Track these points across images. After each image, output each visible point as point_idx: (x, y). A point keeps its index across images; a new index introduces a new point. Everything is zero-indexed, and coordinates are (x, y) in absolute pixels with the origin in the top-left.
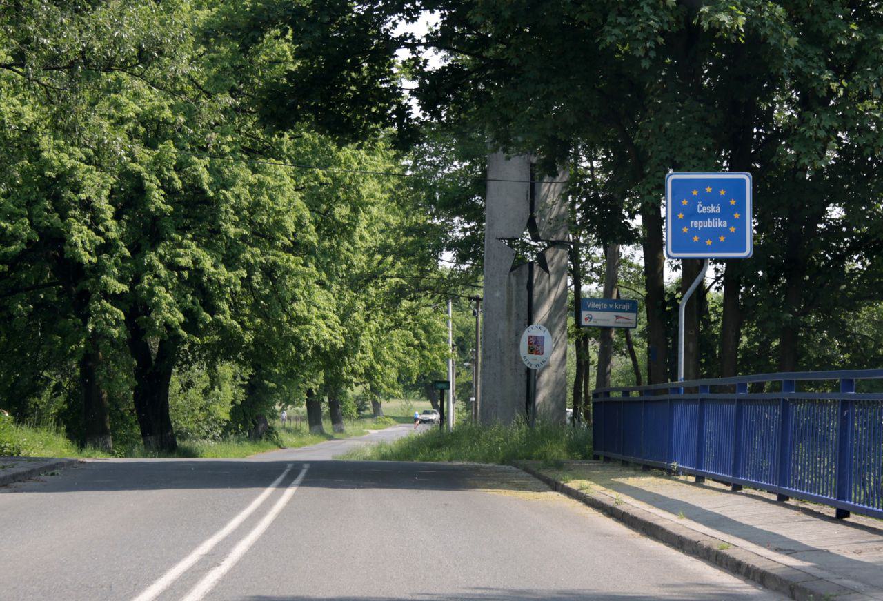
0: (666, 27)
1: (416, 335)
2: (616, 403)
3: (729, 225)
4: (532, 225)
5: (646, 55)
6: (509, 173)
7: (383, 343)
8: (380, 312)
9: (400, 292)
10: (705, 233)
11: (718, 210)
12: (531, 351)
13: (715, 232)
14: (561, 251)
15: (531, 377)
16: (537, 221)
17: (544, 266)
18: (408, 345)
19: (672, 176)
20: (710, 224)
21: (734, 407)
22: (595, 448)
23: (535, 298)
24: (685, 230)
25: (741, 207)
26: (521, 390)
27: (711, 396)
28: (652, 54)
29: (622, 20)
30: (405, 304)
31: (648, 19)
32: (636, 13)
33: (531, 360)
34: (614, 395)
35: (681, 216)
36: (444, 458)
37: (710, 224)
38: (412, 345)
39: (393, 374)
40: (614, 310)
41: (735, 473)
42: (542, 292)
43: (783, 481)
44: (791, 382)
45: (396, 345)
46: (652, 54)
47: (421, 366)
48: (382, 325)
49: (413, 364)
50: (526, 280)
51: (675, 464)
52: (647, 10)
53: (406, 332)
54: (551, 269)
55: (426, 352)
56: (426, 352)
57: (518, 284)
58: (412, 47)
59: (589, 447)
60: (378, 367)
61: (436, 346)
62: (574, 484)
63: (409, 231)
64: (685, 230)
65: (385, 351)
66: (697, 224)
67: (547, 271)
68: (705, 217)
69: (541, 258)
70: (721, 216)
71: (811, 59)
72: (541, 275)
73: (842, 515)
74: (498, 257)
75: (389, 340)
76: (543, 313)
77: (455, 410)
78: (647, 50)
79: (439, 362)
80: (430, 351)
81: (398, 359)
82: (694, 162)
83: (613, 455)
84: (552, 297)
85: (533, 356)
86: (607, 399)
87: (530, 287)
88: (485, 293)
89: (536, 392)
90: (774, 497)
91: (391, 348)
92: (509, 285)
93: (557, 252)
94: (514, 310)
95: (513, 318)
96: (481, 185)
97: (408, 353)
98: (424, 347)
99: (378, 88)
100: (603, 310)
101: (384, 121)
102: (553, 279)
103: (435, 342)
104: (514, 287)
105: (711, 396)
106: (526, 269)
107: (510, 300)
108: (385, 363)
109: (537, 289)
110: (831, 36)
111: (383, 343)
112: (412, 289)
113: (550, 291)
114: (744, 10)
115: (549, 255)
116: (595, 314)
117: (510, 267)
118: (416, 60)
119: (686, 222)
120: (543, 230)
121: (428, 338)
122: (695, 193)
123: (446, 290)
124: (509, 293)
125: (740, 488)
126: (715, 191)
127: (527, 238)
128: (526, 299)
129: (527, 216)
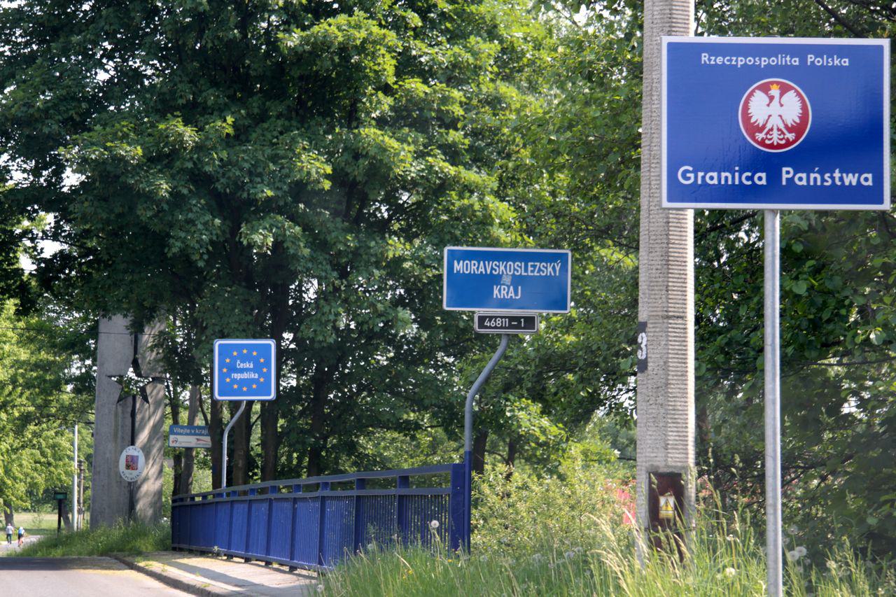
0: (215, 238)
1: (43, 454)
2: (198, 505)
3: (259, 377)
4: (136, 365)
5: (201, 258)
6: (116, 328)
7: (13, 461)
8: (11, 434)
9: (26, 419)
10: (242, 382)
11: (252, 366)
12: (128, 467)
13: (248, 382)
14: (159, 386)
15: (132, 490)
16: (140, 361)
17: (145, 399)
18: (36, 462)
19: (218, 343)
20: (245, 376)
21: (246, 506)
22: (173, 542)
23: (137, 424)
24: (228, 380)
25: (268, 364)
26: (124, 500)
27: (260, 497)
28: (206, 257)
29: (182, 235)
30: (32, 427)
31: (202, 234)
32: (193, 229)
33: (128, 475)
34: (198, 499)
35: (225, 370)
36: (58, 553)
37: (245, 376)
38: (40, 463)
39: (22, 488)
40: (195, 434)
41: (247, 550)
42: (143, 419)
43: (268, 553)
44: (327, 483)
45: (24, 462)
46: (206, 257)
47: (46, 480)
48: (11, 446)
49: (40, 479)
50: (129, 410)
51: (216, 548)
52: (200, 226)
53: (34, 451)
54: (150, 400)
55: (52, 469)
56: (52, 469)
57: (123, 413)
58: (32, 240)
59: (169, 542)
60: (9, 482)
61: (61, 463)
62: (142, 564)
63: (36, 366)
64: (228, 380)
65: (15, 469)
66: (237, 376)
67: (148, 402)
68: (242, 371)
69: (143, 389)
70: (253, 370)
71: (321, 263)
72: (142, 405)
73: (293, 569)
74: (107, 393)
75: (18, 458)
76: (143, 437)
77: (79, 520)
78: (202, 255)
79: (63, 477)
80: (56, 467)
81: (26, 475)
82: (238, 333)
83: (182, 546)
84: (151, 423)
85: (130, 471)
86: (192, 503)
87: (133, 415)
88: (96, 418)
89: (137, 501)
90: (263, 564)
91: (21, 465)
92: (116, 415)
93: (155, 387)
94: (120, 434)
95: (119, 440)
96: (94, 332)
97: (36, 470)
98: (49, 464)
99: (5, 270)
100: (187, 434)
101: (9, 293)
102: (152, 409)
103: (60, 460)
104: (120, 414)
105: (239, 498)
106: (130, 400)
107: (116, 426)
108: (15, 479)
109: (138, 417)
110: (335, 244)
111: (13, 461)
112: (42, 414)
113: (149, 418)
114: (270, 231)
115: (148, 390)
116: (180, 438)
117: (117, 397)
118: (35, 248)
119: (228, 374)
120: (144, 368)
121: (54, 456)
122: (235, 353)
123: (68, 417)
124: (116, 421)
125: (271, 563)
126: (250, 352)
127: (131, 373)
128: (130, 425)
129: (131, 359)
